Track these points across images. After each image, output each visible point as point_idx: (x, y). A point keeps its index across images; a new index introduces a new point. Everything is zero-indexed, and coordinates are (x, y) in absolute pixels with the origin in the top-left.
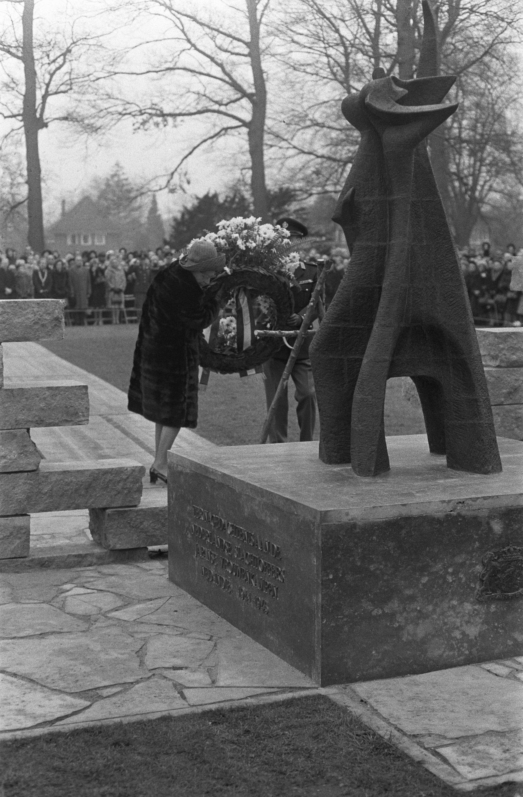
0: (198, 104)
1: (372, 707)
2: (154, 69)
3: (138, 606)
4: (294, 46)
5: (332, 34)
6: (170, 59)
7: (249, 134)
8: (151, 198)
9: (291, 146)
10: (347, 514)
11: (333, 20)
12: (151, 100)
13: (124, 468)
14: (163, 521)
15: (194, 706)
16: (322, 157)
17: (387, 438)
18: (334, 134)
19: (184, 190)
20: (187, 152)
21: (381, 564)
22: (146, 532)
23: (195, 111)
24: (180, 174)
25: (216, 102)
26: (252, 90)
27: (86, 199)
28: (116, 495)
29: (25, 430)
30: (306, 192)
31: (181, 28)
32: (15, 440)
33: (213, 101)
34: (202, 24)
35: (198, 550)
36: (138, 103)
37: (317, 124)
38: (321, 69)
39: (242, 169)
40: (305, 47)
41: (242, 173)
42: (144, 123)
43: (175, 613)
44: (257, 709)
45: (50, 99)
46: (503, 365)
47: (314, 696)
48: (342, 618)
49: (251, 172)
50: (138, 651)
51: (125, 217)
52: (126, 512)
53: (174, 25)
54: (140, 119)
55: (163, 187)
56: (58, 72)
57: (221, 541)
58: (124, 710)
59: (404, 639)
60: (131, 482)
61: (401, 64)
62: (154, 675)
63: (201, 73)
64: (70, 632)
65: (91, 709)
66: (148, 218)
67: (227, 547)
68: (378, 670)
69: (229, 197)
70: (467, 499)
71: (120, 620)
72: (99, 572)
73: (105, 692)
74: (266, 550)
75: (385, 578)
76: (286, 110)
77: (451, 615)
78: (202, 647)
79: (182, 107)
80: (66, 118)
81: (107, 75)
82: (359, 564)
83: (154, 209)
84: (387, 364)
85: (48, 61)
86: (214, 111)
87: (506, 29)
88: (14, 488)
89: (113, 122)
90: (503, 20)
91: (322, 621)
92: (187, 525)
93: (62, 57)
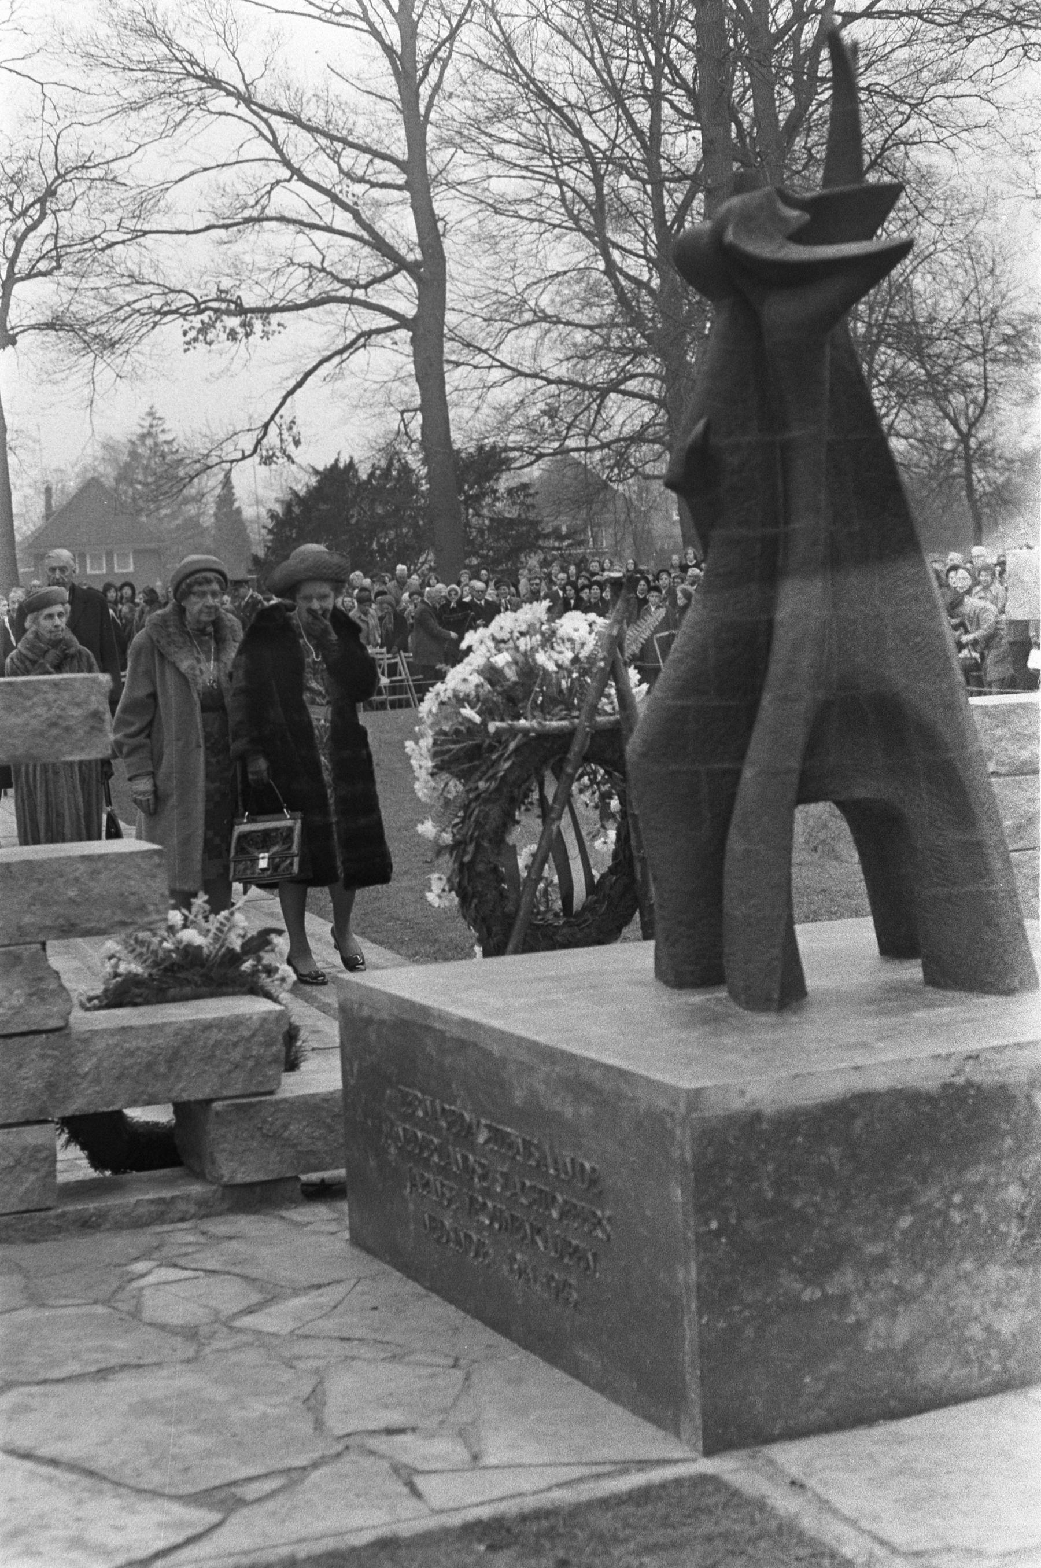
0: (310, 286)
1: (816, 1495)
2: (221, 222)
3: (297, 1302)
4: (493, 167)
5: (569, 138)
6: (251, 201)
7: (413, 341)
8: (221, 476)
9: (495, 363)
10: (742, 1093)
11: (567, 111)
12: (218, 284)
13: (243, 1015)
14: (329, 1120)
15: (442, 1511)
16: (559, 381)
17: (798, 928)
18: (579, 336)
19: (289, 457)
20: (292, 383)
21: (815, 1194)
22: (294, 1146)
23: (304, 301)
24: (280, 427)
25: (346, 282)
26: (416, 255)
27: (91, 486)
28: (230, 1072)
29: (39, 946)
30: (530, 451)
31: (271, 138)
32: (19, 968)
33: (339, 280)
34: (311, 129)
35: (413, 1179)
36: (191, 290)
37: (546, 318)
38: (548, 208)
39: (402, 412)
40: (515, 165)
41: (403, 420)
42: (204, 329)
43: (376, 1312)
44: (576, 1512)
45: (18, 289)
46: (1003, 770)
47: (691, 1478)
48: (740, 1312)
49: (419, 417)
50: (308, 1399)
51: (173, 516)
52: (251, 1105)
53: (256, 134)
54: (196, 321)
55: (247, 453)
56: (32, 235)
57: (465, 1159)
58: (294, 1528)
59: (869, 1348)
60: (261, 1044)
61: (709, 193)
62: (347, 1448)
63: (313, 226)
64: (159, 1365)
65: (224, 1530)
66: (215, 515)
67: (479, 1171)
68: (819, 1414)
69: (379, 468)
70: (984, 1050)
71: (260, 1332)
72: (203, 1233)
73: (251, 1491)
74: (566, 1173)
75: (826, 1222)
76: (484, 291)
77: (962, 1293)
78: (440, 1382)
79: (279, 295)
80: (50, 326)
81: (129, 236)
82: (770, 1195)
83: (227, 497)
84: (794, 778)
85: (10, 215)
86: (342, 300)
87: (909, 117)
88: (20, 1066)
89: (144, 330)
90: (901, 99)
91: (700, 1317)
92: (385, 1128)
93: (38, 206)
